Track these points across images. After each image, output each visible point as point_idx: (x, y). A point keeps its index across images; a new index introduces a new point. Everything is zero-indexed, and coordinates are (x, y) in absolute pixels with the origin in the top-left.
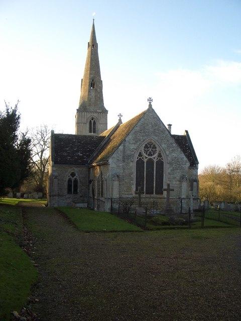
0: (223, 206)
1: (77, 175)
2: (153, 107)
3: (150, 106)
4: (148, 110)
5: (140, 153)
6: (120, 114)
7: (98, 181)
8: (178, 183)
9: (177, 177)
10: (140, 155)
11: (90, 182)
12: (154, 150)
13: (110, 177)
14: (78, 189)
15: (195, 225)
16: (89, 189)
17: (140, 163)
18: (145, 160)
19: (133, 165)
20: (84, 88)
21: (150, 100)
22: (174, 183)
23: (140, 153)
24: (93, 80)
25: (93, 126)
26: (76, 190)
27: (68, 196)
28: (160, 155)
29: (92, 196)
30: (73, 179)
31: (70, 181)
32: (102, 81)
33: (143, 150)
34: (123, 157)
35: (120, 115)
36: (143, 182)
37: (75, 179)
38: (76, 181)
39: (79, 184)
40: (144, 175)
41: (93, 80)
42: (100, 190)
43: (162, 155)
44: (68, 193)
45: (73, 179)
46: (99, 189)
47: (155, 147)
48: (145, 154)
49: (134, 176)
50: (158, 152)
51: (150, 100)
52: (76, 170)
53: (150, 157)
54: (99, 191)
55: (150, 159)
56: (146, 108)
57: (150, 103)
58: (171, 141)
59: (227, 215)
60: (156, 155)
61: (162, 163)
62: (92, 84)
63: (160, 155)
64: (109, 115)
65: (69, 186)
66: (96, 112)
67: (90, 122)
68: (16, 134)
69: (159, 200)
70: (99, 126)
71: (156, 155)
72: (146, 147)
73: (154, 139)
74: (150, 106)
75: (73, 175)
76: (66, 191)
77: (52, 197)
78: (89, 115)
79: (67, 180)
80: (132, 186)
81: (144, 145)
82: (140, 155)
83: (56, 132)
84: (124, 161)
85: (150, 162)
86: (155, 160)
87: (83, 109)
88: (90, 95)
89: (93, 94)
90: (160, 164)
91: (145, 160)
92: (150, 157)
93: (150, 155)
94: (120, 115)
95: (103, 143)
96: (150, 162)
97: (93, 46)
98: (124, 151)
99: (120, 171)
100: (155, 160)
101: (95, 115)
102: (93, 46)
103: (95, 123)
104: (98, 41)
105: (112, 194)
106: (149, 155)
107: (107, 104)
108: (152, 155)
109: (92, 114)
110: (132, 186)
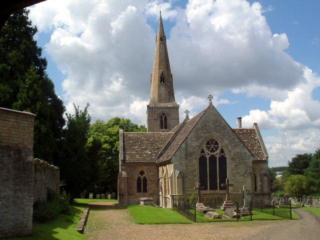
9: (241, 173)
10: (203, 151)
12: (216, 146)
17: (202, 160)
18: (208, 157)
24: (162, 75)
28: (222, 151)
30: (142, 177)
31: (139, 179)
37: (145, 177)
39: (149, 182)
41: (162, 75)
44: (139, 190)
45: (142, 177)
47: (217, 143)
49: (197, 173)
55: (213, 156)
60: (218, 151)
61: (225, 158)
63: (222, 151)
71: (218, 151)
72: (208, 143)
73: (216, 136)
79: (136, 178)
85: (213, 158)
86: (218, 156)
90: (223, 160)
91: (208, 157)
93: (212, 151)
96: (213, 158)
100: (218, 156)
106: (211, 151)
108: (214, 151)
110: (135, 182)
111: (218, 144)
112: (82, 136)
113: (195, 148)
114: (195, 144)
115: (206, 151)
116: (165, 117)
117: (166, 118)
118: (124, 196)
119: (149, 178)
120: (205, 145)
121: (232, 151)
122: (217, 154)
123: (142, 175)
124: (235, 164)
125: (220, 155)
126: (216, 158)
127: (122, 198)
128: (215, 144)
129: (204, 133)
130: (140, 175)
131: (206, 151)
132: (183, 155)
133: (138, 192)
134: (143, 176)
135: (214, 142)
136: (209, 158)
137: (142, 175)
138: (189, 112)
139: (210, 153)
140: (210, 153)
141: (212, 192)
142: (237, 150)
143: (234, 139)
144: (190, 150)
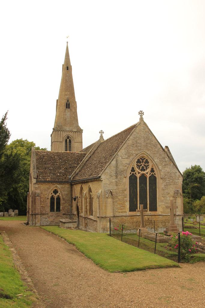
1: (59, 192)
2: (145, 120)
3: (141, 119)
4: (139, 124)
5: (133, 168)
6: (102, 131)
7: (86, 199)
8: (172, 198)
9: (171, 193)
10: (133, 170)
11: (75, 199)
12: (147, 164)
13: (103, 194)
14: (61, 207)
16: (72, 207)
17: (133, 179)
18: (138, 176)
19: (126, 182)
20: (59, 108)
21: (141, 113)
22: (168, 198)
23: (133, 168)
24: (68, 101)
25: (68, 142)
26: (58, 209)
27: (50, 214)
28: (152, 170)
30: (56, 196)
31: (52, 198)
32: (76, 102)
33: (136, 166)
34: (116, 173)
35: (102, 132)
36: (137, 198)
37: (58, 196)
38: (58, 199)
39: (62, 202)
40: (137, 191)
41: (68, 101)
42: (88, 208)
43: (155, 169)
44: (52, 209)
45: (56, 196)
46: (87, 206)
47: (147, 162)
48: (137, 170)
49: (127, 192)
50: (150, 167)
51: (141, 113)
52: (59, 187)
53: (143, 172)
54: (86, 209)
55: (143, 175)
56: (136, 120)
57: (141, 116)
58: (163, 156)
59: (120, 211)
60: (149, 170)
61: (155, 178)
62: (67, 104)
63: (152, 170)
64: (84, 134)
66: (72, 131)
67: (66, 140)
68: (7, 128)
69: (154, 218)
70: (75, 145)
71: (149, 170)
72: (138, 161)
73: (148, 153)
74: (141, 119)
75: (56, 192)
76: (48, 209)
77: (34, 216)
78: (65, 134)
79: (50, 197)
80: (126, 203)
81: (136, 160)
82: (133, 170)
84: (117, 177)
85: (143, 177)
86: (148, 176)
87: (57, 130)
90: (153, 179)
91: (138, 176)
92: (143, 172)
93: (143, 170)
94: (102, 132)
95: (85, 159)
96: (143, 177)
97: (67, 68)
98: (117, 167)
99: (113, 188)
100: (148, 176)
101: (70, 134)
102: (67, 68)
103: (70, 141)
105: (106, 213)
106: (141, 170)
107: (82, 124)
108: (144, 170)
109: (68, 133)
110: (126, 203)
111: (148, 163)
112: (142, 114)
113: (126, 166)
114: (127, 161)
115: (137, 170)
116: (70, 140)
117: (70, 141)
118: (37, 216)
119: (62, 197)
120: (136, 163)
121: (163, 170)
122: (147, 173)
123: (56, 194)
124: (165, 184)
125: (150, 174)
126: (146, 178)
127: (35, 218)
128: (145, 163)
129: (135, 150)
130: (53, 194)
131: (137, 170)
132: (113, 173)
133: (51, 211)
134: (57, 195)
135: (144, 161)
136: (150, 177)
137: (56, 194)
138: (103, 133)
139: (140, 172)
140: (140, 172)
141: (153, 213)
142: (167, 169)
143: (164, 158)
144: (121, 167)
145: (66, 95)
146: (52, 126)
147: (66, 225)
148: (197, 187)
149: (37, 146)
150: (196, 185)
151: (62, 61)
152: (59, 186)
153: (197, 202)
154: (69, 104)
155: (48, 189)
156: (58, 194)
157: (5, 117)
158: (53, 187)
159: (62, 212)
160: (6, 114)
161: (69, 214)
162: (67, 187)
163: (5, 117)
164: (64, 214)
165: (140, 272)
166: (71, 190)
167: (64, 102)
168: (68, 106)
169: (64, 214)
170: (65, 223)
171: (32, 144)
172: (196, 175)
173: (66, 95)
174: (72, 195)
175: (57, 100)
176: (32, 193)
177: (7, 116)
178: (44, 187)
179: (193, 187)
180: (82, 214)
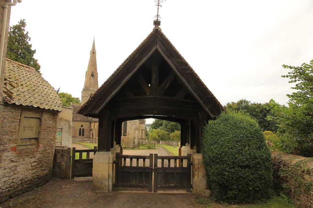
0: (148, 163)
11: (91, 130)
15: (27, 184)
21: (157, 23)
26: (83, 135)
29: (92, 137)
30: (82, 128)
31: (80, 129)
38: (83, 129)
39: (85, 131)
44: (80, 135)
45: (82, 128)
51: (157, 23)
52: (84, 123)
56: (149, 29)
62: (92, 74)
65: (80, 132)
75: (82, 126)
83: (27, 29)
88: (91, 81)
89: (92, 80)
97: (93, 53)
102: (93, 53)
104: (96, 50)
130: (81, 127)
133: (79, 135)
145: (92, 69)
146: (82, 87)
147: (85, 141)
148: (174, 125)
149: (75, 98)
150: (174, 123)
151: (91, 49)
152: (84, 123)
153: (172, 134)
154: (93, 75)
155: (78, 124)
156: (83, 127)
157: (59, 90)
158: (81, 124)
159: (85, 136)
160: (59, 89)
161: (89, 137)
162: (88, 123)
163: (59, 90)
164: (86, 137)
165: (34, 119)
166: (90, 126)
167: (90, 73)
168: (92, 75)
169: (86, 137)
170: (85, 140)
171: (70, 96)
172: (244, 104)
173: (92, 69)
174: (90, 128)
175: (86, 72)
176: (70, 133)
177: (60, 90)
178: (76, 123)
179: (172, 125)
180: (94, 138)
